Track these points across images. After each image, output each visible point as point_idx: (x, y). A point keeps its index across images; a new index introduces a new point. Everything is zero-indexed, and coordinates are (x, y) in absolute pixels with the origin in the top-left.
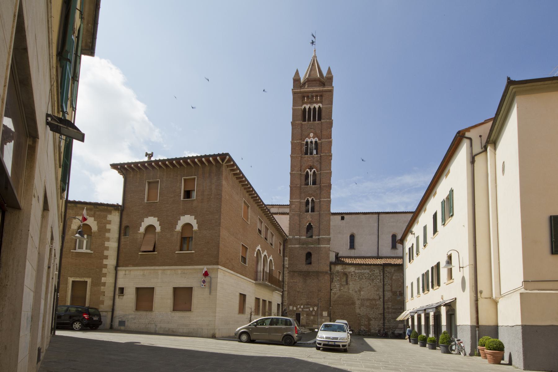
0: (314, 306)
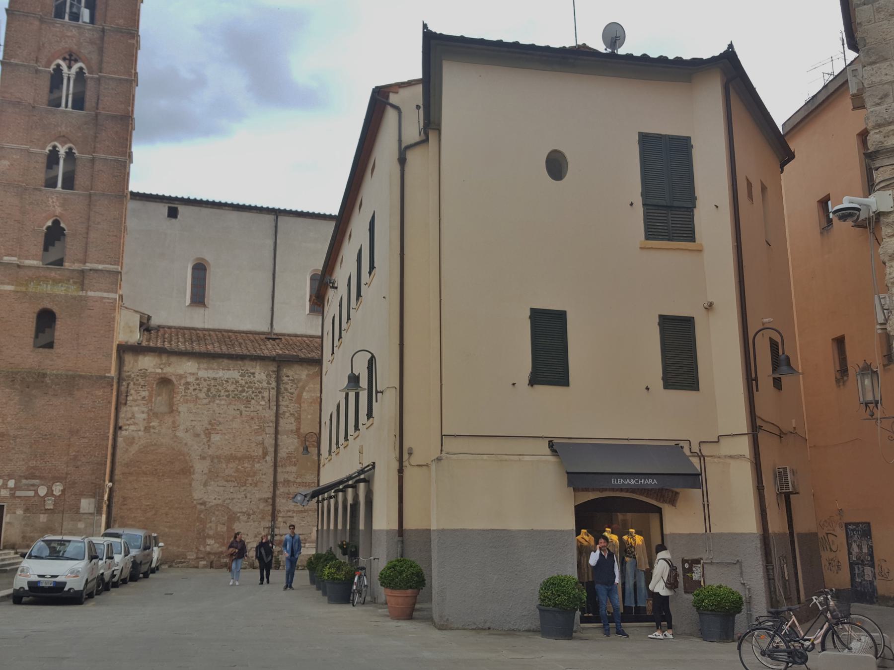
0: (51, 479)
